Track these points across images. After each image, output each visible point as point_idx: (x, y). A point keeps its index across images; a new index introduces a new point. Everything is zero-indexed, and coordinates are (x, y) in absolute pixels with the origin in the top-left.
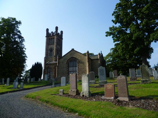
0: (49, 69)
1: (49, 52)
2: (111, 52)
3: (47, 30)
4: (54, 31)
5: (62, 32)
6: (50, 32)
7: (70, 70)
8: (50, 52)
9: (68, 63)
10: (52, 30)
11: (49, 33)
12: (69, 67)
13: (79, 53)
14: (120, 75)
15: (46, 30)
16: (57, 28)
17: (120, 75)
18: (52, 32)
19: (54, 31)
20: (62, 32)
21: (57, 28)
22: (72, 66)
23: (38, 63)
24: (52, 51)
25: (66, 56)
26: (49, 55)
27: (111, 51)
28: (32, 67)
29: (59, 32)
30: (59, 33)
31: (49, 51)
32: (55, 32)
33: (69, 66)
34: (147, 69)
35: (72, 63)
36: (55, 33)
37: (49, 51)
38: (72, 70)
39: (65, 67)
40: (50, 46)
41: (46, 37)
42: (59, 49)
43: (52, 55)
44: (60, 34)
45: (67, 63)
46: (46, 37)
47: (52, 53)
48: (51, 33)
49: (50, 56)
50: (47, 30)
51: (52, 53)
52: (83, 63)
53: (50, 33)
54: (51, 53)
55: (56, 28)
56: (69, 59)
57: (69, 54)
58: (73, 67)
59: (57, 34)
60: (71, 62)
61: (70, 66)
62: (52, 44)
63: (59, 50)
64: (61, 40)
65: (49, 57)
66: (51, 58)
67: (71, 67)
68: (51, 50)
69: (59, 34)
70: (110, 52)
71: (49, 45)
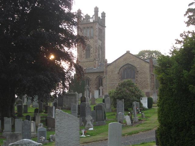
5: (104, 14)
16: (96, 10)
19: (91, 14)
21: (96, 10)
25: (117, 62)
29: (100, 15)
32: (93, 16)
39: (116, 78)
42: (100, 45)
56: (122, 67)
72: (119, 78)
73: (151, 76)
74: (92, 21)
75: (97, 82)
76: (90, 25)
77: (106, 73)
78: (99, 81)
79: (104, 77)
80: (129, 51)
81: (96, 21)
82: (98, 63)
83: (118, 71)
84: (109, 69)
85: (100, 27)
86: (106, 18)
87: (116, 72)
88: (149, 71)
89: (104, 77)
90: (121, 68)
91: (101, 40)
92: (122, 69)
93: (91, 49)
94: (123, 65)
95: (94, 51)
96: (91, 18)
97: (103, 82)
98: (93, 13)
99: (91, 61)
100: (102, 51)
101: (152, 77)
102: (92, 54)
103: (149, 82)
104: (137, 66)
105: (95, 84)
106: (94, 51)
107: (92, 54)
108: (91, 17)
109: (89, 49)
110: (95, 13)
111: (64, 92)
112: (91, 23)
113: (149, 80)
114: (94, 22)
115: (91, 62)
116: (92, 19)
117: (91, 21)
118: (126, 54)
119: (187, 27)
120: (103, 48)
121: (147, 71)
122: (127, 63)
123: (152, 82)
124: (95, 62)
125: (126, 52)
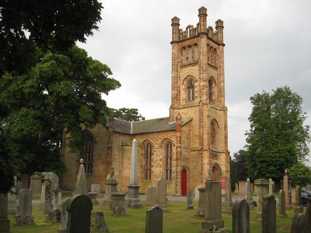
3: (175, 22)
4: (194, 21)
5: (220, 24)
6: (183, 27)
14: (57, 150)
16: (203, 13)
17: (57, 150)
18: (189, 27)
19: (194, 21)
21: (203, 13)
28: (99, 13)
29: (211, 22)
30: (211, 28)
32: (198, 24)
34: (45, 65)
36: (186, 32)
48: (187, 28)
50: (175, 22)
53: (184, 30)
59: (207, 33)
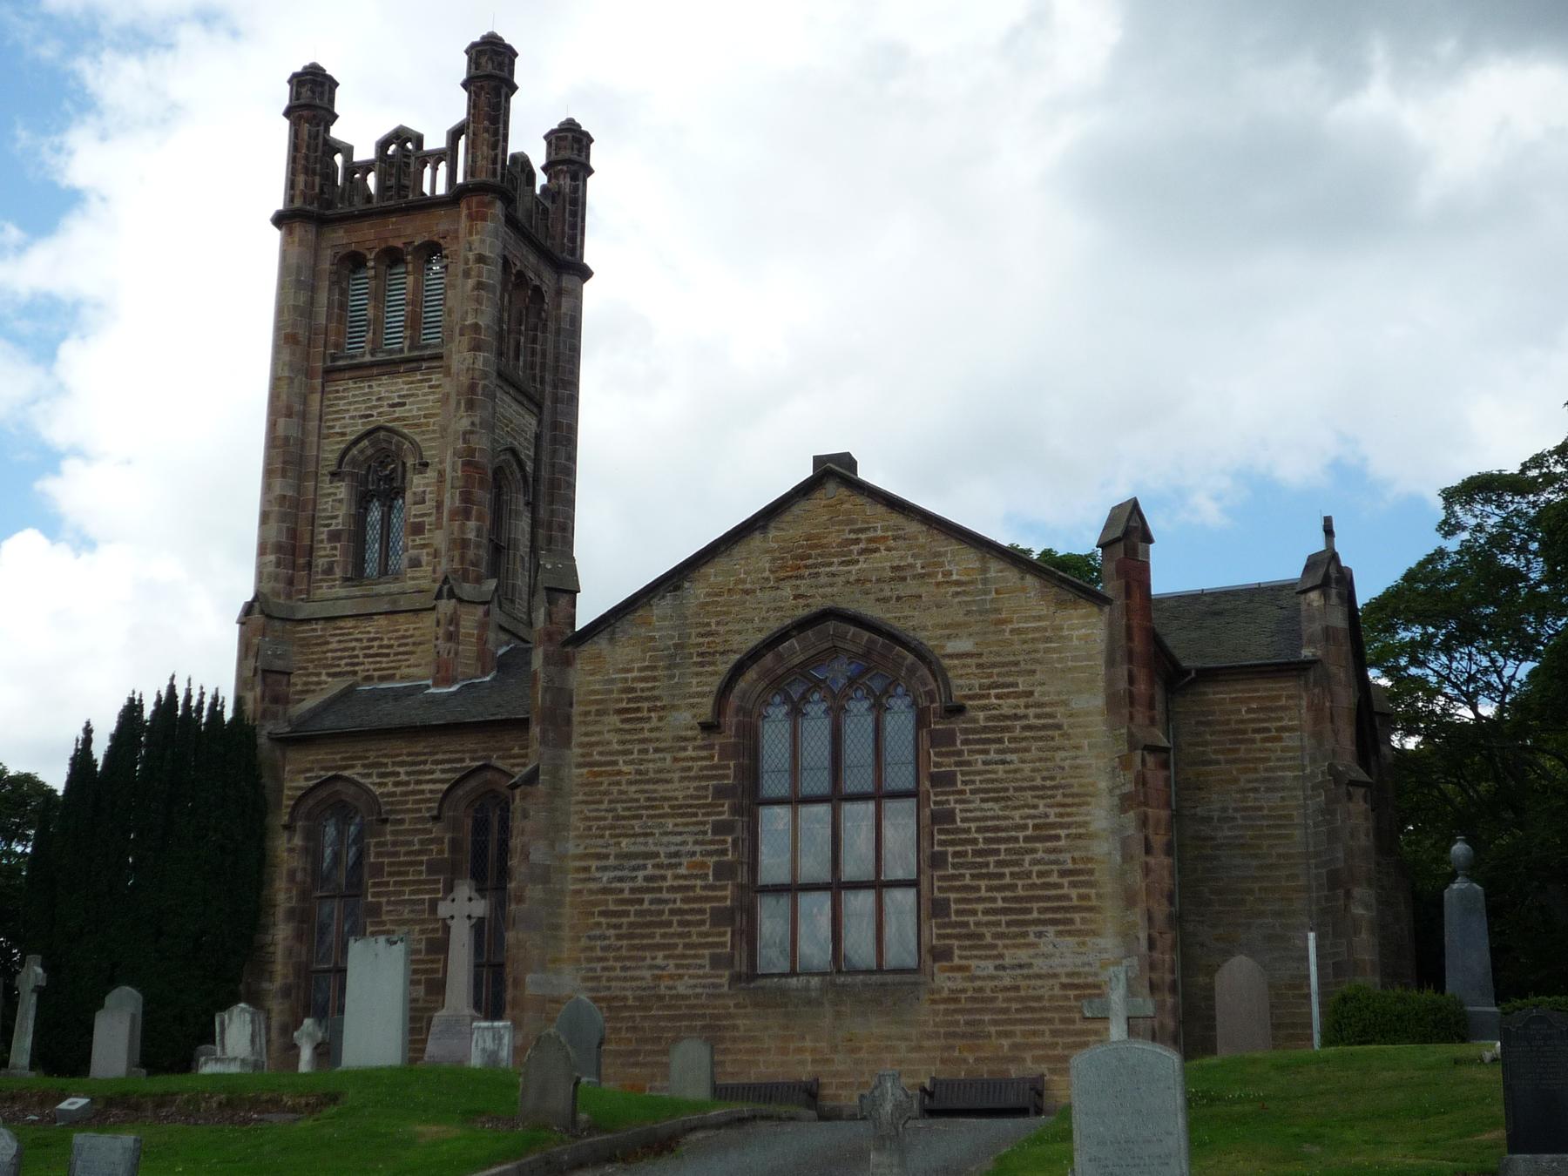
0: (331, 831)
1: (336, 501)
2: (1452, 545)
3: (312, 95)
5: (570, 144)
6: (358, 129)
7: (773, 866)
8: (363, 500)
9: (730, 728)
10: (399, 96)
11: (348, 151)
12: (747, 797)
13: (951, 547)
15: (460, 67)
16: (491, 70)
19: (438, 113)
20: (570, 144)
21: (491, 70)
22: (817, 781)
23: (167, 704)
24: (400, 492)
25: (696, 591)
26: (328, 553)
27: (1449, 527)
29: (527, 137)
30: (522, 162)
31: (342, 490)
32: (454, 135)
33: (751, 773)
35: (816, 730)
36: (449, 154)
37: (330, 495)
38: (814, 866)
39: (679, 790)
40: (356, 407)
41: (280, 220)
42: (513, 451)
43: (384, 571)
44: (541, 179)
45: (707, 727)
46: (280, 220)
47: (386, 522)
49: (357, 575)
50: (312, 95)
51: (386, 522)
52: (1048, 729)
54: (375, 514)
55: (296, 94)
56: (754, 656)
57: (756, 558)
58: (836, 797)
59: (497, 181)
60: (796, 712)
61: (773, 784)
62: (391, 366)
63: (529, 478)
64: (559, 292)
65: (332, 593)
66: (371, 628)
67: (796, 800)
68: (379, 471)
69: (531, 176)
70: (1435, 541)
71: (330, 373)
72: (720, 792)
73: (1125, 763)
74: (441, 190)
75: (455, 845)
76: (413, 231)
77: (559, 717)
78: (481, 827)
79: (532, 778)
80: (847, 461)
81: (483, 177)
82: (483, 626)
83: (709, 702)
84: (583, 678)
85: (527, 260)
86: (596, 190)
87: (684, 719)
88: (1099, 701)
89: (532, 778)
90: (738, 670)
91: (533, 402)
92: (751, 674)
93: (418, 483)
94: (774, 625)
95: (439, 506)
96: (438, 156)
97: (515, 842)
98: (457, 108)
99: (403, 604)
100: (543, 513)
101: (1141, 780)
102: (418, 529)
103: (1104, 849)
104: (952, 647)
105: (433, 868)
106: (439, 506)
107: (418, 529)
108: (435, 140)
109: (389, 479)
110: (473, 105)
111: (1541, 621)
112: (435, 202)
113: (1100, 815)
114: (457, 194)
115: (405, 625)
116: (443, 167)
117: (435, 182)
118: (803, 491)
119: (1121, 495)
120: (554, 485)
121: (1081, 702)
122: (818, 604)
123: (1148, 850)
124: (454, 620)
125: (807, 472)
